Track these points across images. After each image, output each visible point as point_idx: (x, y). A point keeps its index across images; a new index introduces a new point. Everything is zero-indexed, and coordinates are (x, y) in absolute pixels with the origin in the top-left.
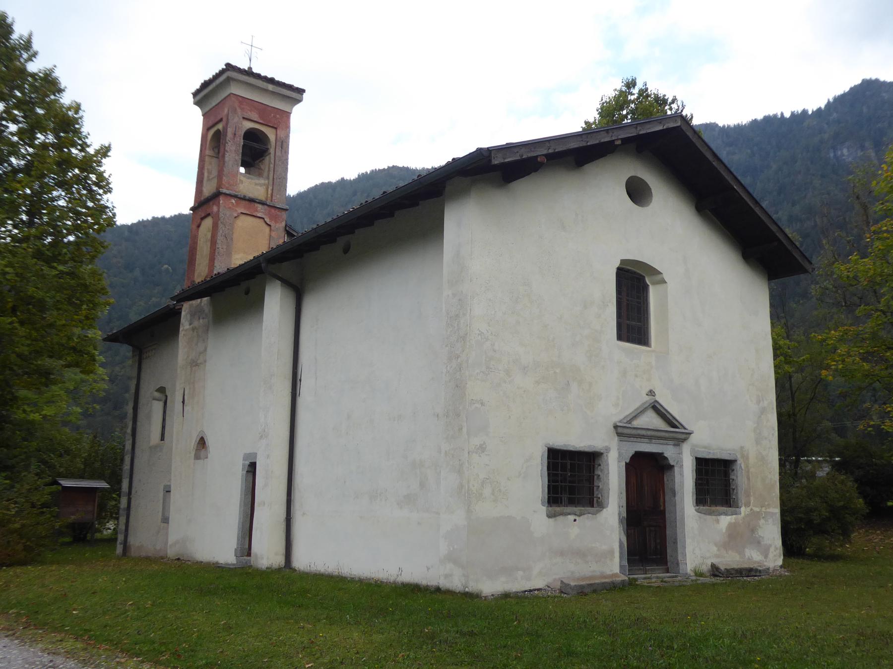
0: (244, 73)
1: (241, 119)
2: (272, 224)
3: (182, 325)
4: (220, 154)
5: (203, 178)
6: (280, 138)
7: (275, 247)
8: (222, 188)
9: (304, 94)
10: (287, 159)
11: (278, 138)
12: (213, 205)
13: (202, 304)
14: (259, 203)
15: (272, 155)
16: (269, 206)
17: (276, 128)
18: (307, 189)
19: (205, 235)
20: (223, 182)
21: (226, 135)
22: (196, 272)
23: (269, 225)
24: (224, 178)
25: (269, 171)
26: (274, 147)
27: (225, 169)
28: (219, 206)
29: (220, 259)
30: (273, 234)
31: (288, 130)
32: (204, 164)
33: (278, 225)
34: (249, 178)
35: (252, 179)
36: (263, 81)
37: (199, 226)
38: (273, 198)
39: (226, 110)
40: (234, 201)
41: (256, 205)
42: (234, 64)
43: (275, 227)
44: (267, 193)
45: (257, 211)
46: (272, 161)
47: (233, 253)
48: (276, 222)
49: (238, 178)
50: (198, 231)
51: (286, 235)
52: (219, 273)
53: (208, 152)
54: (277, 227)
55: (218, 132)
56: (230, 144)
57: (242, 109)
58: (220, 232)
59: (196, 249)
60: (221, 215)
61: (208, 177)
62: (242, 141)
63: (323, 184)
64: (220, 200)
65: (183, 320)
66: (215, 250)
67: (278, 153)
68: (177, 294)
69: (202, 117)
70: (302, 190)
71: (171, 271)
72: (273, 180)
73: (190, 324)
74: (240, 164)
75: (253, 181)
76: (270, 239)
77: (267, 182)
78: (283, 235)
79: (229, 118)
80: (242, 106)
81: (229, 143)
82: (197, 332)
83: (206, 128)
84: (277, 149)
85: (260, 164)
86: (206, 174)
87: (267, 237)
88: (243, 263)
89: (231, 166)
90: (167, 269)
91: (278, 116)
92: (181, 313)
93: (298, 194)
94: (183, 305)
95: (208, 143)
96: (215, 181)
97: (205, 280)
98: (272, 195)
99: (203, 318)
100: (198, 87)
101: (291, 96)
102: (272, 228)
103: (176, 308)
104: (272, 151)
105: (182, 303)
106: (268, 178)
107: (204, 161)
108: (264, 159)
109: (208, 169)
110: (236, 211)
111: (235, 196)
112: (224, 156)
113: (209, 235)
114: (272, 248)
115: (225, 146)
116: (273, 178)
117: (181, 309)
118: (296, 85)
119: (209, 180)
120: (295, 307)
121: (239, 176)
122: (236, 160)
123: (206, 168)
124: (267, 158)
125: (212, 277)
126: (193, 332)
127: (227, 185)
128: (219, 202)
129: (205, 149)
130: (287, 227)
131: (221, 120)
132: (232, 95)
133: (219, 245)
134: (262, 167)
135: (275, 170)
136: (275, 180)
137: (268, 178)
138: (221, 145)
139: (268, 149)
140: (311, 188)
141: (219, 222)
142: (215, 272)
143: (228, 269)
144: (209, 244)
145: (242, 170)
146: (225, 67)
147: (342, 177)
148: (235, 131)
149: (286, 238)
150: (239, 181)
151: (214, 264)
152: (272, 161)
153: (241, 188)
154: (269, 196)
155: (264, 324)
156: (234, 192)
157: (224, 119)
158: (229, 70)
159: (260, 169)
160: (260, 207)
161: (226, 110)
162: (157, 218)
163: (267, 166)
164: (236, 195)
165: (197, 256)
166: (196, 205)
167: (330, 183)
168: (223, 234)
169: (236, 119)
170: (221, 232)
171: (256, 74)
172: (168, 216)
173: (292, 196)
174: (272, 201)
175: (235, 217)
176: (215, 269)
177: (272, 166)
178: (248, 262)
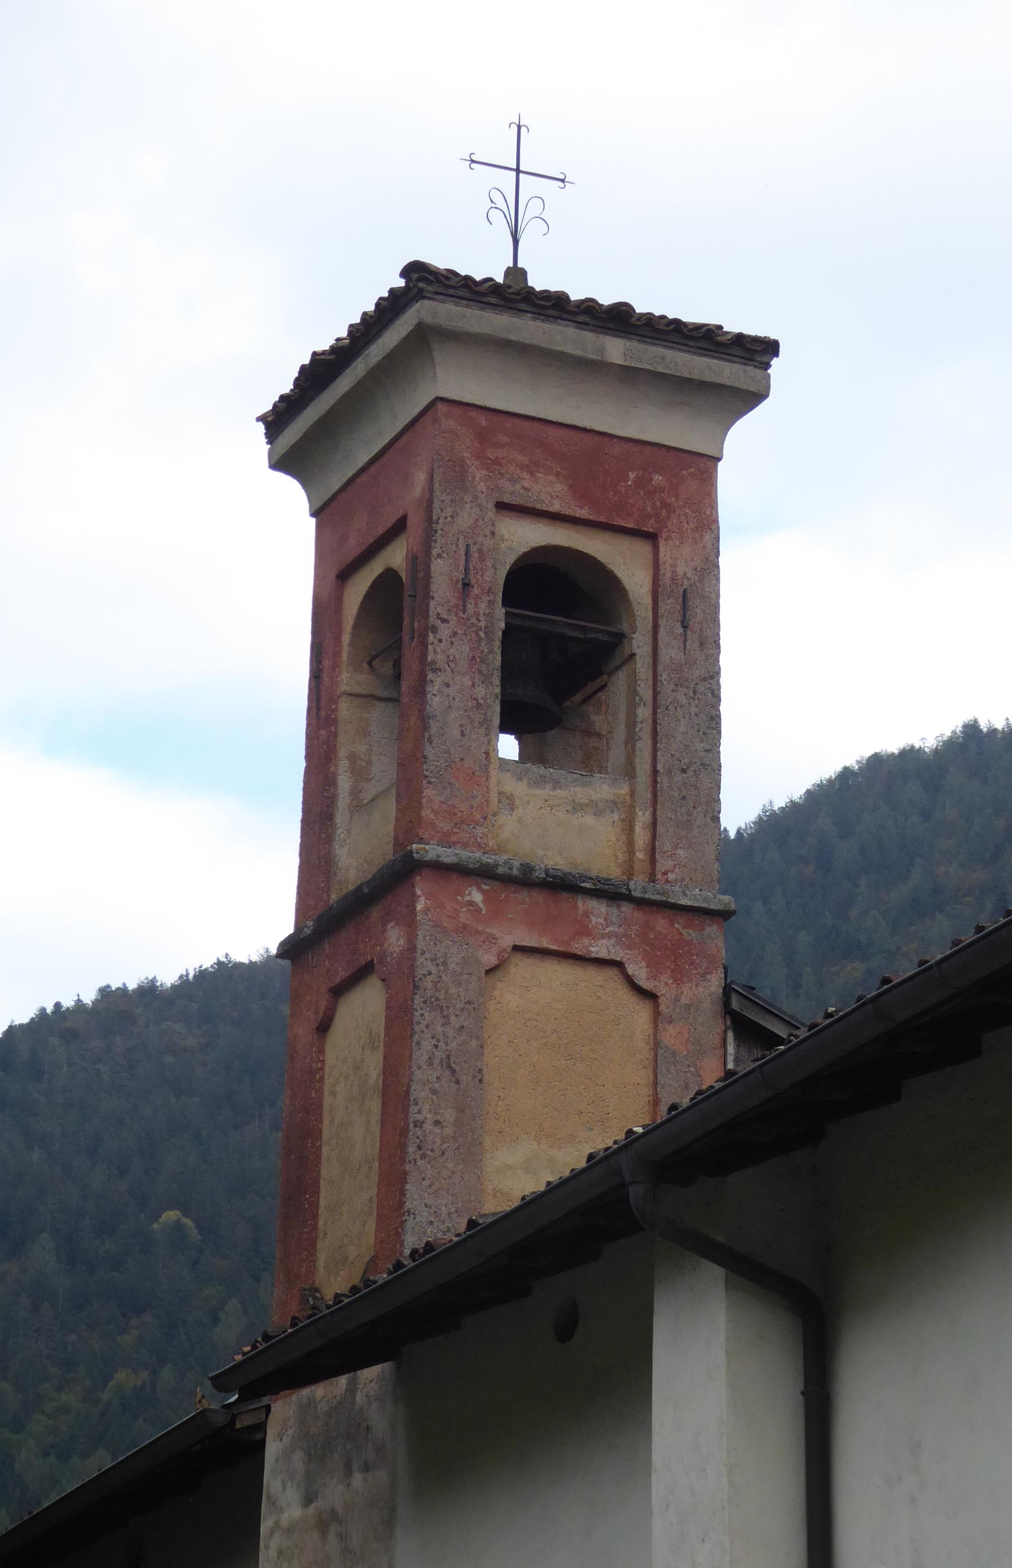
0: (493, 300)
1: (491, 513)
2: (663, 986)
3: (273, 1503)
4: (406, 685)
5: (331, 801)
6: (673, 579)
7: (685, 1102)
8: (421, 841)
9: (774, 362)
10: (713, 676)
11: (666, 579)
12: (385, 922)
13: (359, 1397)
14: (597, 893)
15: (642, 666)
16: (642, 903)
17: (652, 538)
18: (802, 791)
19: (357, 1067)
20: (426, 813)
21: (428, 596)
22: (319, 1244)
23: (650, 996)
24: (429, 792)
25: (631, 738)
26: (649, 626)
27: (429, 751)
28: (411, 925)
29: (429, 1173)
30: (670, 1034)
31: (708, 537)
32: (335, 734)
33: (687, 992)
34: (540, 782)
35: (556, 784)
36: (581, 325)
37: (324, 1027)
38: (660, 867)
39: (420, 478)
40: (477, 897)
41: (585, 904)
42: (440, 261)
43: (677, 999)
44: (631, 843)
45: (586, 931)
46: (645, 691)
47: (487, 1142)
48: (679, 977)
49: (493, 781)
50: (321, 1051)
51: (730, 1036)
52: (429, 1247)
53: (347, 679)
54: (684, 1000)
55: (389, 578)
56: (444, 631)
57: (493, 465)
58: (423, 1049)
59: (320, 1137)
60: (424, 964)
61: (355, 793)
62: (500, 612)
63: (876, 761)
64: (414, 894)
65: (272, 1481)
66: (404, 1132)
67: (670, 652)
68: (239, 1358)
69: (313, 521)
70: (780, 802)
71: (195, 1235)
72: (655, 782)
73: (308, 1500)
74: (497, 721)
75: (558, 792)
76: (656, 1060)
77: (624, 790)
78: (717, 1041)
79: (436, 511)
80: (492, 453)
81: (442, 626)
82: (342, 1537)
83: (332, 574)
84: (662, 633)
85: (589, 708)
86: (344, 783)
87: (645, 1053)
88: (542, 1188)
89: (456, 733)
90: (178, 1226)
91: (658, 478)
92: (261, 1445)
93: (760, 822)
94: (268, 1409)
95: (346, 638)
96: (389, 807)
97: (367, 1282)
98: (653, 849)
99: (366, 1468)
100: (287, 387)
101: (709, 377)
102: (662, 1008)
103: (238, 1426)
104: (640, 643)
105: (265, 1400)
106: (629, 772)
107: (335, 721)
108: (603, 687)
109: (352, 757)
110: (492, 939)
111: (484, 873)
112: (420, 691)
113: (374, 1065)
114: (673, 1107)
115: (424, 644)
116: (655, 772)
117: (261, 1427)
118: (733, 325)
119: (358, 807)
120: (801, 1386)
121: (494, 773)
122: (479, 706)
123: (342, 752)
124: (620, 679)
125: (399, 1265)
126: (324, 1533)
127: (444, 825)
128: (412, 906)
129: (336, 665)
130: (734, 996)
131: (400, 526)
132: (440, 406)
133: (423, 1111)
134: (598, 721)
135: (661, 731)
136: (663, 781)
137: (629, 772)
138: (406, 639)
139: (620, 637)
140: (820, 786)
141: (418, 1000)
142: (412, 1241)
143: (472, 1224)
144: (375, 1106)
145: (508, 746)
146: (401, 283)
147: (967, 717)
148: (467, 569)
149: (731, 1049)
150: (494, 799)
151: (402, 1204)
152: (645, 691)
153: (505, 834)
154: (640, 855)
155: (659, 1482)
156: (478, 855)
157: (415, 521)
158: (420, 295)
159: (589, 732)
160: (598, 910)
161: (420, 478)
162: (123, 991)
163: (622, 717)
164: (488, 865)
165: (324, 1171)
166: (307, 931)
167: (909, 754)
168: (439, 1054)
169: (465, 518)
170: (427, 1044)
171: (546, 295)
172: (168, 978)
173: (732, 834)
174: (652, 879)
175: (489, 971)
176: (410, 1224)
177: (643, 713)
178: (563, 1183)
